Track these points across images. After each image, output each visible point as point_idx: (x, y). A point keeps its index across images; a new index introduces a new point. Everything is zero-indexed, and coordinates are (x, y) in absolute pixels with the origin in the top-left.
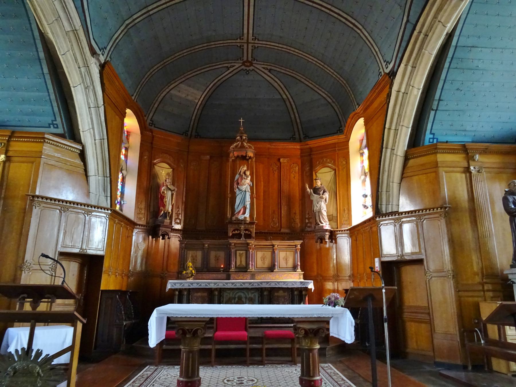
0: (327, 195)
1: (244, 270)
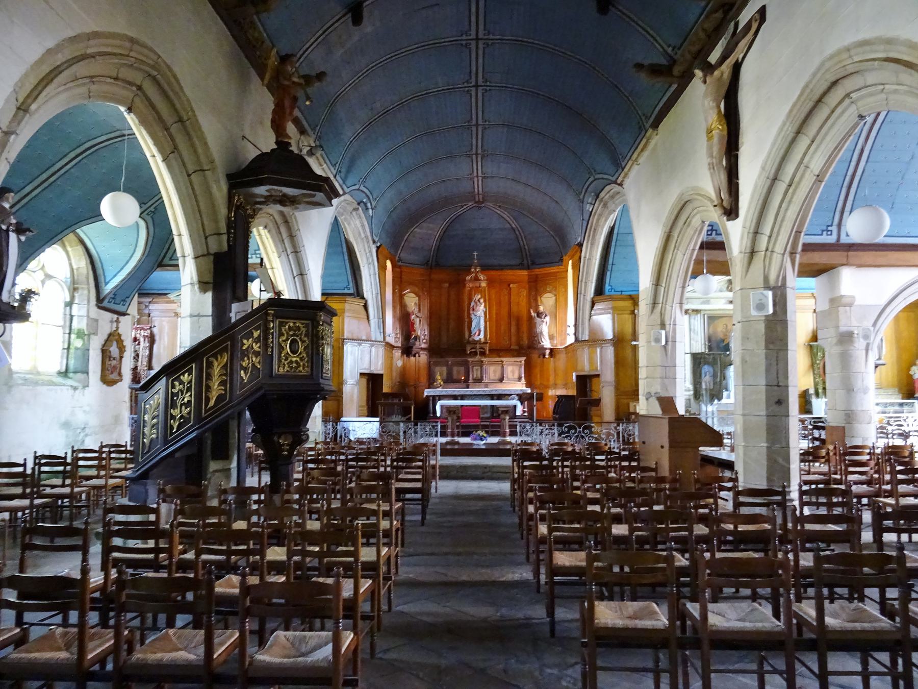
0: (547, 319)
1: (479, 381)
